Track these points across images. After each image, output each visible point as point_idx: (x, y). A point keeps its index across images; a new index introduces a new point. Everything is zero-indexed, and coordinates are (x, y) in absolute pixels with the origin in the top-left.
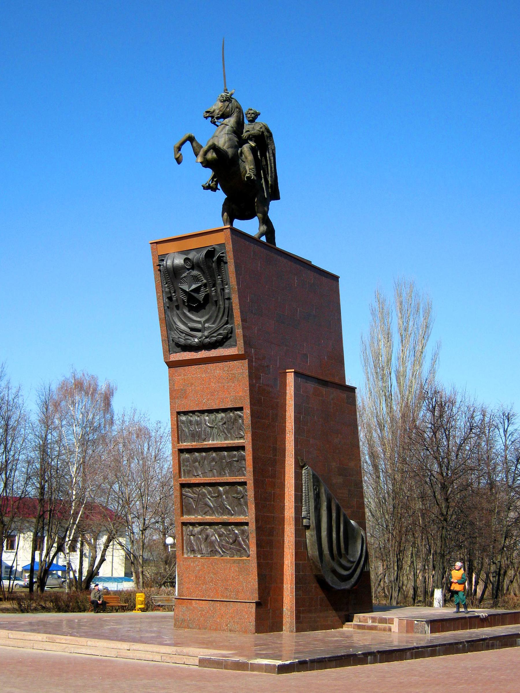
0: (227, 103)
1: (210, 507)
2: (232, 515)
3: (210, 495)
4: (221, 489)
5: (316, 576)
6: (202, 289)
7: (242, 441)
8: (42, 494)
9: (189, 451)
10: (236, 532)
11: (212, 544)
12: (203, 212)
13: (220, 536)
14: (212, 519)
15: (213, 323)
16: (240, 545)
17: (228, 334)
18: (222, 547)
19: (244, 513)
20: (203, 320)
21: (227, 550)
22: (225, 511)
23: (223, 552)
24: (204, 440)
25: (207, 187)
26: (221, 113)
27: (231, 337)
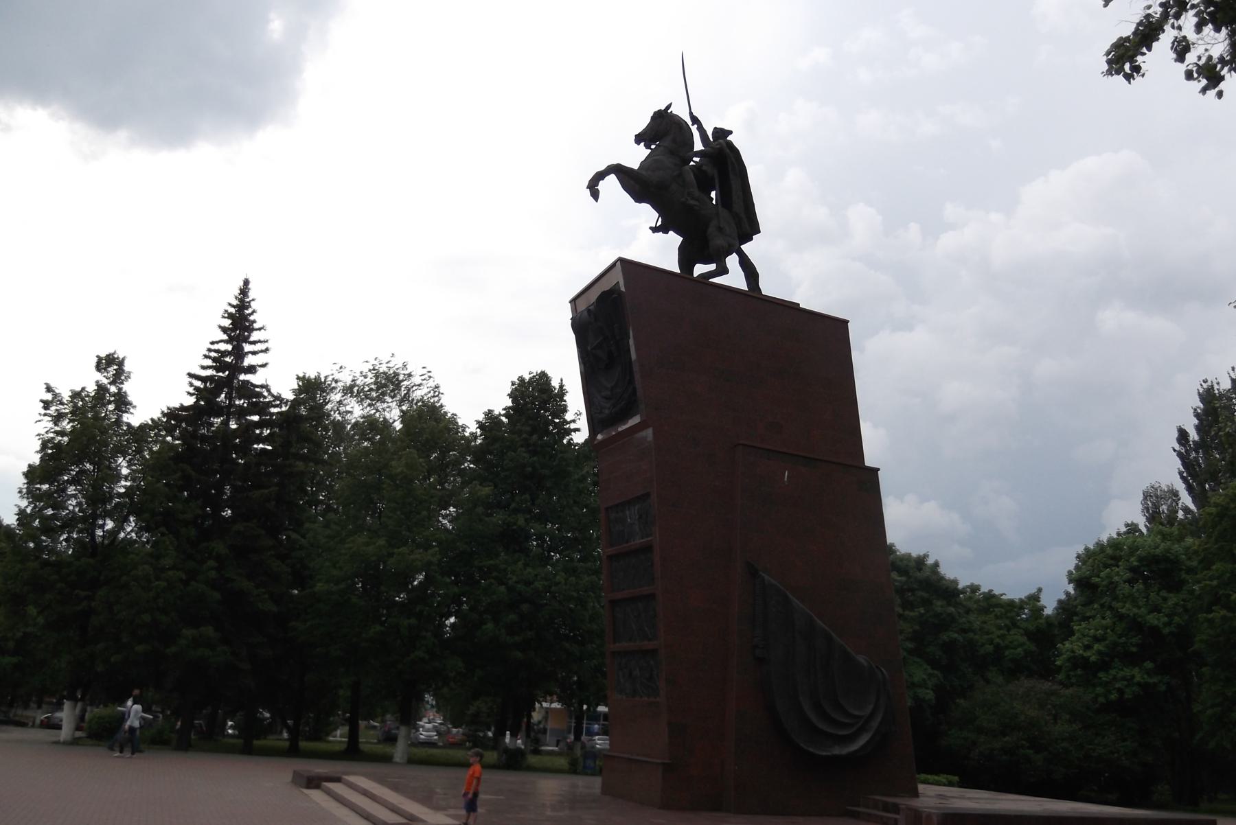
25: (655, 230)
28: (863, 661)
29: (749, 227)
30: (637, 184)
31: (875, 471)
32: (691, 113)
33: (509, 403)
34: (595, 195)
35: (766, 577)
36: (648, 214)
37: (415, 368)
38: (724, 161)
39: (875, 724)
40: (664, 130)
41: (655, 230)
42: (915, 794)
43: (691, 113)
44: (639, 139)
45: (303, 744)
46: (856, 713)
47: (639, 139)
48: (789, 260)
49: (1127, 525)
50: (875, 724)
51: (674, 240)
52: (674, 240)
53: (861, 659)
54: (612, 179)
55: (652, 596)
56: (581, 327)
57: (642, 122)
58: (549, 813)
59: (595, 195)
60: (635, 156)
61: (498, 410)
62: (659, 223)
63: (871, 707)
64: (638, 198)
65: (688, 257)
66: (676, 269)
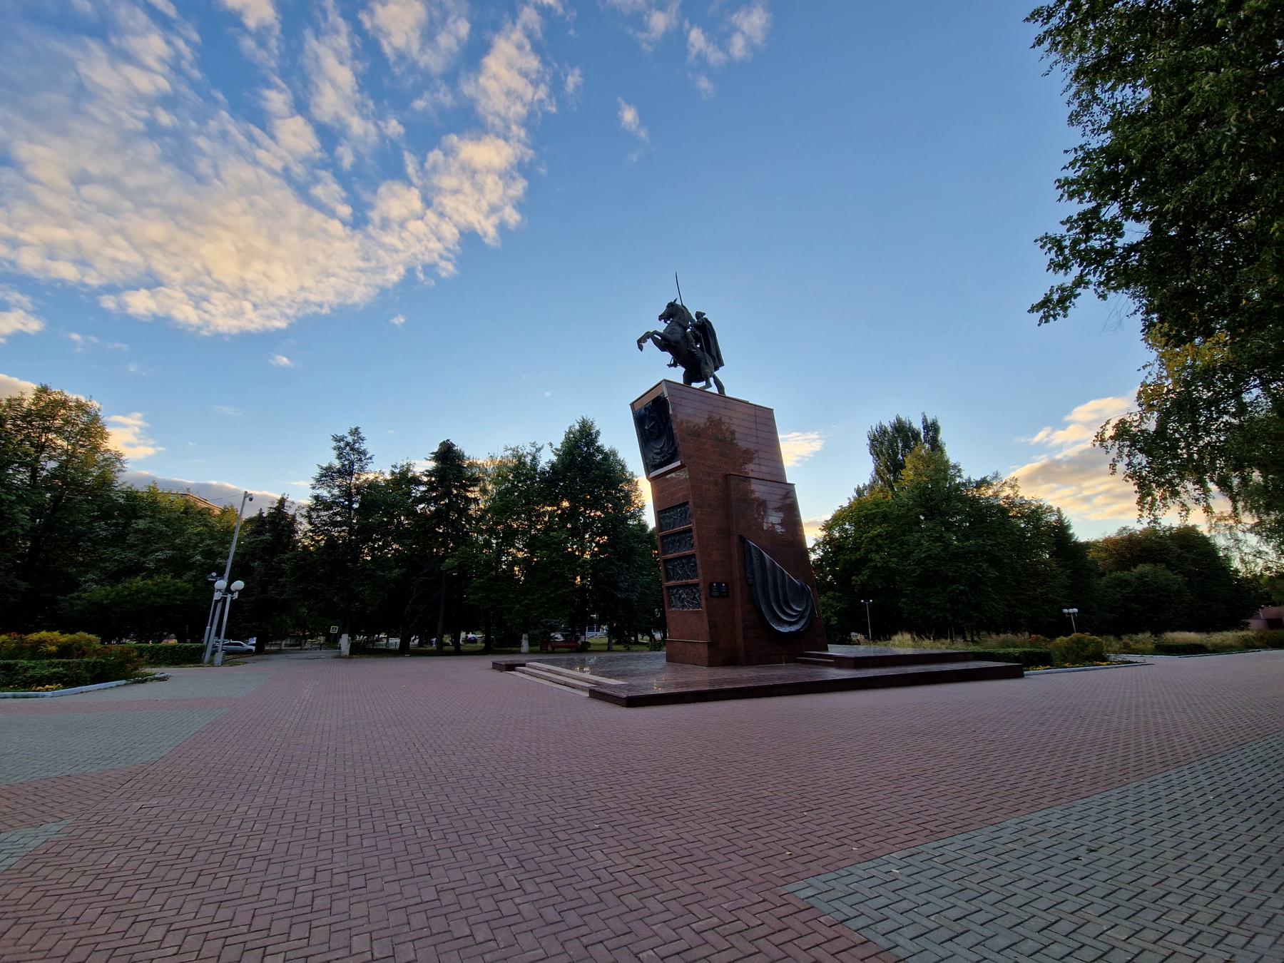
12: (661, 370)
22: (688, 577)
25: (670, 366)
29: (718, 363)
30: (664, 343)
34: (641, 348)
36: (668, 357)
37: (467, 454)
38: (704, 330)
40: (674, 312)
41: (670, 366)
44: (661, 318)
45: (614, 647)
47: (661, 318)
48: (738, 379)
50: (807, 613)
51: (681, 370)
52: (681, 370)
54: (650, 341)
56: (640, 420)
57: (663, 309)
58: (1064, 467)
59: (641, 348)
60: (661, 327)
61: (965, 475)
64: (663, 348)
65: (689, 378)
66: (682, 382)
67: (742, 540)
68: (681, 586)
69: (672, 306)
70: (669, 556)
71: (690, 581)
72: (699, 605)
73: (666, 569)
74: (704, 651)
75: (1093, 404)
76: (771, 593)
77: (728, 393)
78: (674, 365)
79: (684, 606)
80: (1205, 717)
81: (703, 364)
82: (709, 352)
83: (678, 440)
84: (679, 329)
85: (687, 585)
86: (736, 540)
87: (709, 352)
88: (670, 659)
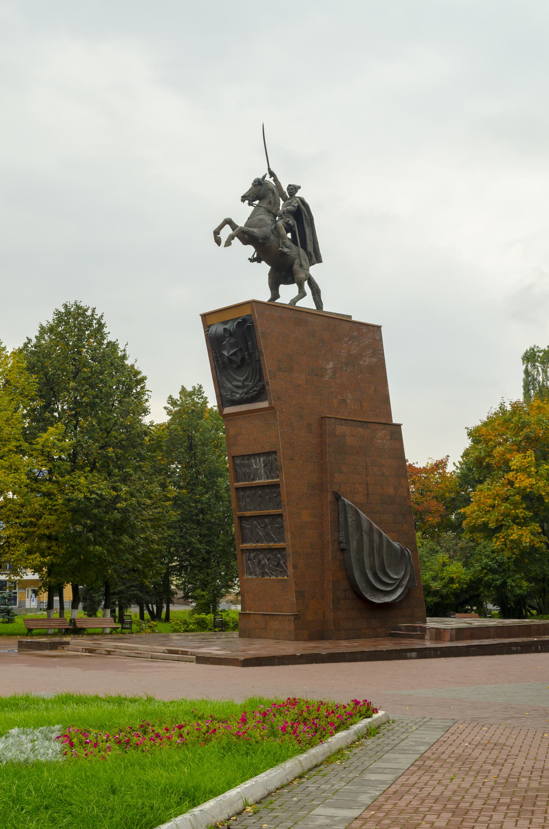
0: (259, 187)
1: (260, 536)
2: (276, 542)
3: (259, 525)
4: (267, 520)
5: (84, 629)
6: (239, 354)
7: (278, 480)
8: (122, 533)
9: (244, 489)
10: (279, 556)
11: (263, 566)
12: (247, 281)
13: (268, 560)
14: (261, 546)
15: (250, 382)
16: (282, 567)
17: (260, 390)
18: (270, 569)
19: (283, 540)
20: (242, 379)
21: (273, 571)
22: (271, 540)
23: (271, 573)
24: (253, 480)
25: (252, 260)
26: (255, 196)
27: (263, 392)
28: (396, 545)
29: (315, 257)
31: (399, 426)
32: (269, 169)
33: (422, 467)
35: (346, 500)
39: (405, 583)
40: (261, 192)
42: (425, 622)
43: (269, 169)
46: (395, 577)
48: (343, 284)
49: (247, 198)
50: (405, 583)
53: (396, 544)
55: (280, 515)
56: (215, 343)
57: (246, 187)
60: (242, 213)
62: (255, 256)
63: (403, 573)
67: (337, 497)
68: (262, 550)
69: (259, 183)
70: (248, 514)
71: (272, 544)
72: (284, 572)
73: (242, 528)
74: (290, 626)
75: (380, 602)
76: (366, 559)
77: (327, 308)
78: (257, 260)
79: (264, 574)
80: (371, 554)
81: (296, 267)
82: (304, 246)
83: (267, 377)
84: (268, 219)
85: (271, 550)
86: (330, 497)
87: (304, 246)
88: (241, 636)
